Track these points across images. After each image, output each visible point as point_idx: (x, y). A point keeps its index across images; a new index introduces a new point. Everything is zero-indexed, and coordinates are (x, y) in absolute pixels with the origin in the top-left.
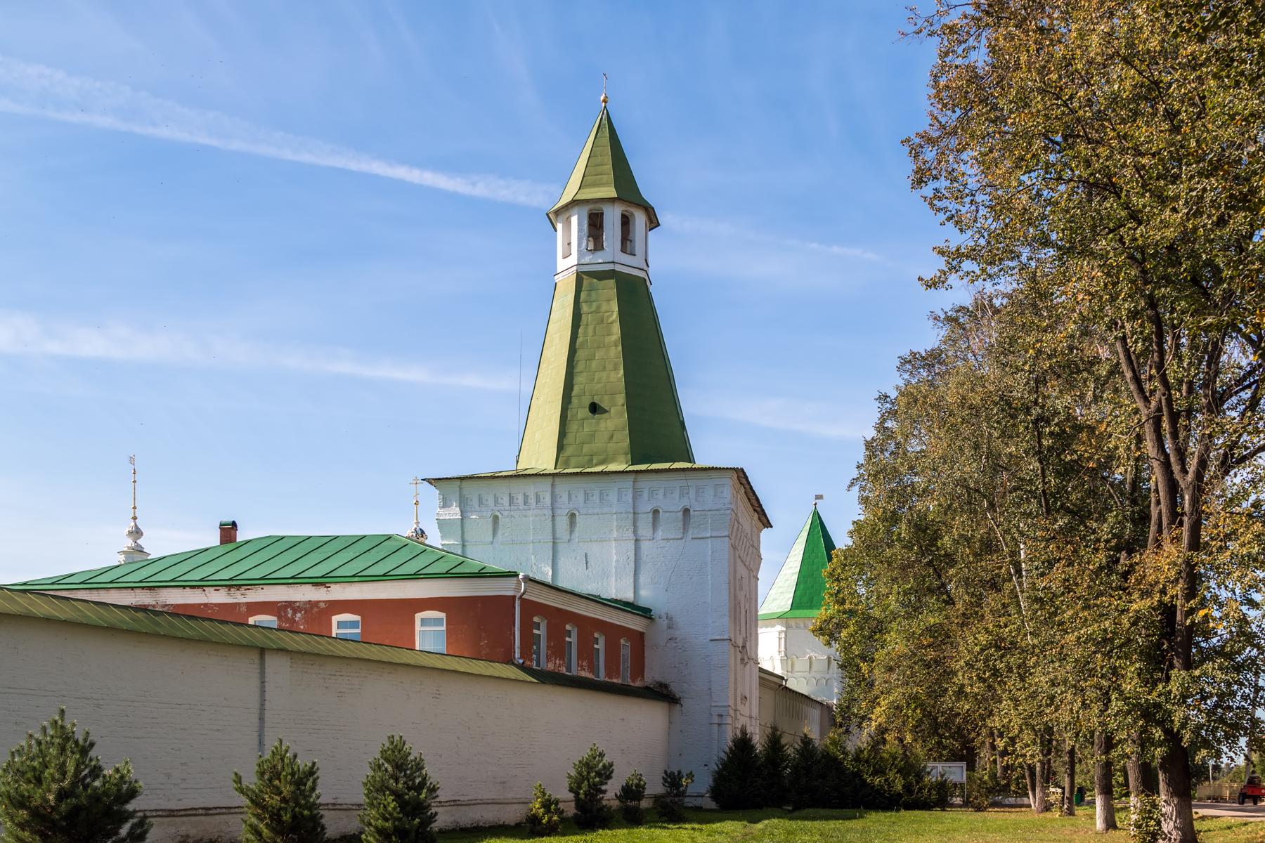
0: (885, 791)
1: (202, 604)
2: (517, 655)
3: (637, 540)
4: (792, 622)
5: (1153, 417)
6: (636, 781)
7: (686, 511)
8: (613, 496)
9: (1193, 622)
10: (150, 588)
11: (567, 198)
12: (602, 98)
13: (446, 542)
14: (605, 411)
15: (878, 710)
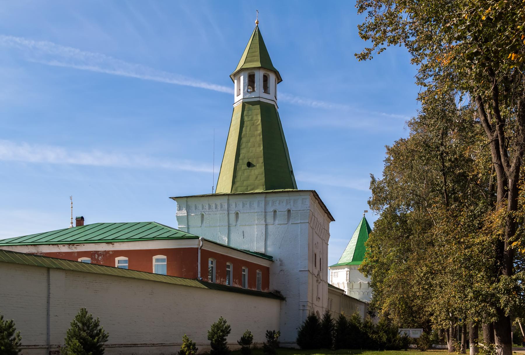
0: (378, 341)
1: (58, 252)
2: (199, 276)
3: (266, 225)
4: (353, 267)
5: (495, 140)
6: (248, 335)
7: (289, 211)
8: (255, 205)
9: (510, 248)
10: (34, 245)
11: (238, 68)
12: (256, 22)
13: (180, 226)
14: (254, 166)
15: (385, 305)
